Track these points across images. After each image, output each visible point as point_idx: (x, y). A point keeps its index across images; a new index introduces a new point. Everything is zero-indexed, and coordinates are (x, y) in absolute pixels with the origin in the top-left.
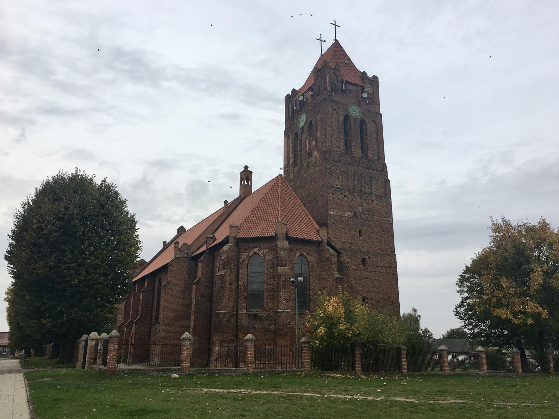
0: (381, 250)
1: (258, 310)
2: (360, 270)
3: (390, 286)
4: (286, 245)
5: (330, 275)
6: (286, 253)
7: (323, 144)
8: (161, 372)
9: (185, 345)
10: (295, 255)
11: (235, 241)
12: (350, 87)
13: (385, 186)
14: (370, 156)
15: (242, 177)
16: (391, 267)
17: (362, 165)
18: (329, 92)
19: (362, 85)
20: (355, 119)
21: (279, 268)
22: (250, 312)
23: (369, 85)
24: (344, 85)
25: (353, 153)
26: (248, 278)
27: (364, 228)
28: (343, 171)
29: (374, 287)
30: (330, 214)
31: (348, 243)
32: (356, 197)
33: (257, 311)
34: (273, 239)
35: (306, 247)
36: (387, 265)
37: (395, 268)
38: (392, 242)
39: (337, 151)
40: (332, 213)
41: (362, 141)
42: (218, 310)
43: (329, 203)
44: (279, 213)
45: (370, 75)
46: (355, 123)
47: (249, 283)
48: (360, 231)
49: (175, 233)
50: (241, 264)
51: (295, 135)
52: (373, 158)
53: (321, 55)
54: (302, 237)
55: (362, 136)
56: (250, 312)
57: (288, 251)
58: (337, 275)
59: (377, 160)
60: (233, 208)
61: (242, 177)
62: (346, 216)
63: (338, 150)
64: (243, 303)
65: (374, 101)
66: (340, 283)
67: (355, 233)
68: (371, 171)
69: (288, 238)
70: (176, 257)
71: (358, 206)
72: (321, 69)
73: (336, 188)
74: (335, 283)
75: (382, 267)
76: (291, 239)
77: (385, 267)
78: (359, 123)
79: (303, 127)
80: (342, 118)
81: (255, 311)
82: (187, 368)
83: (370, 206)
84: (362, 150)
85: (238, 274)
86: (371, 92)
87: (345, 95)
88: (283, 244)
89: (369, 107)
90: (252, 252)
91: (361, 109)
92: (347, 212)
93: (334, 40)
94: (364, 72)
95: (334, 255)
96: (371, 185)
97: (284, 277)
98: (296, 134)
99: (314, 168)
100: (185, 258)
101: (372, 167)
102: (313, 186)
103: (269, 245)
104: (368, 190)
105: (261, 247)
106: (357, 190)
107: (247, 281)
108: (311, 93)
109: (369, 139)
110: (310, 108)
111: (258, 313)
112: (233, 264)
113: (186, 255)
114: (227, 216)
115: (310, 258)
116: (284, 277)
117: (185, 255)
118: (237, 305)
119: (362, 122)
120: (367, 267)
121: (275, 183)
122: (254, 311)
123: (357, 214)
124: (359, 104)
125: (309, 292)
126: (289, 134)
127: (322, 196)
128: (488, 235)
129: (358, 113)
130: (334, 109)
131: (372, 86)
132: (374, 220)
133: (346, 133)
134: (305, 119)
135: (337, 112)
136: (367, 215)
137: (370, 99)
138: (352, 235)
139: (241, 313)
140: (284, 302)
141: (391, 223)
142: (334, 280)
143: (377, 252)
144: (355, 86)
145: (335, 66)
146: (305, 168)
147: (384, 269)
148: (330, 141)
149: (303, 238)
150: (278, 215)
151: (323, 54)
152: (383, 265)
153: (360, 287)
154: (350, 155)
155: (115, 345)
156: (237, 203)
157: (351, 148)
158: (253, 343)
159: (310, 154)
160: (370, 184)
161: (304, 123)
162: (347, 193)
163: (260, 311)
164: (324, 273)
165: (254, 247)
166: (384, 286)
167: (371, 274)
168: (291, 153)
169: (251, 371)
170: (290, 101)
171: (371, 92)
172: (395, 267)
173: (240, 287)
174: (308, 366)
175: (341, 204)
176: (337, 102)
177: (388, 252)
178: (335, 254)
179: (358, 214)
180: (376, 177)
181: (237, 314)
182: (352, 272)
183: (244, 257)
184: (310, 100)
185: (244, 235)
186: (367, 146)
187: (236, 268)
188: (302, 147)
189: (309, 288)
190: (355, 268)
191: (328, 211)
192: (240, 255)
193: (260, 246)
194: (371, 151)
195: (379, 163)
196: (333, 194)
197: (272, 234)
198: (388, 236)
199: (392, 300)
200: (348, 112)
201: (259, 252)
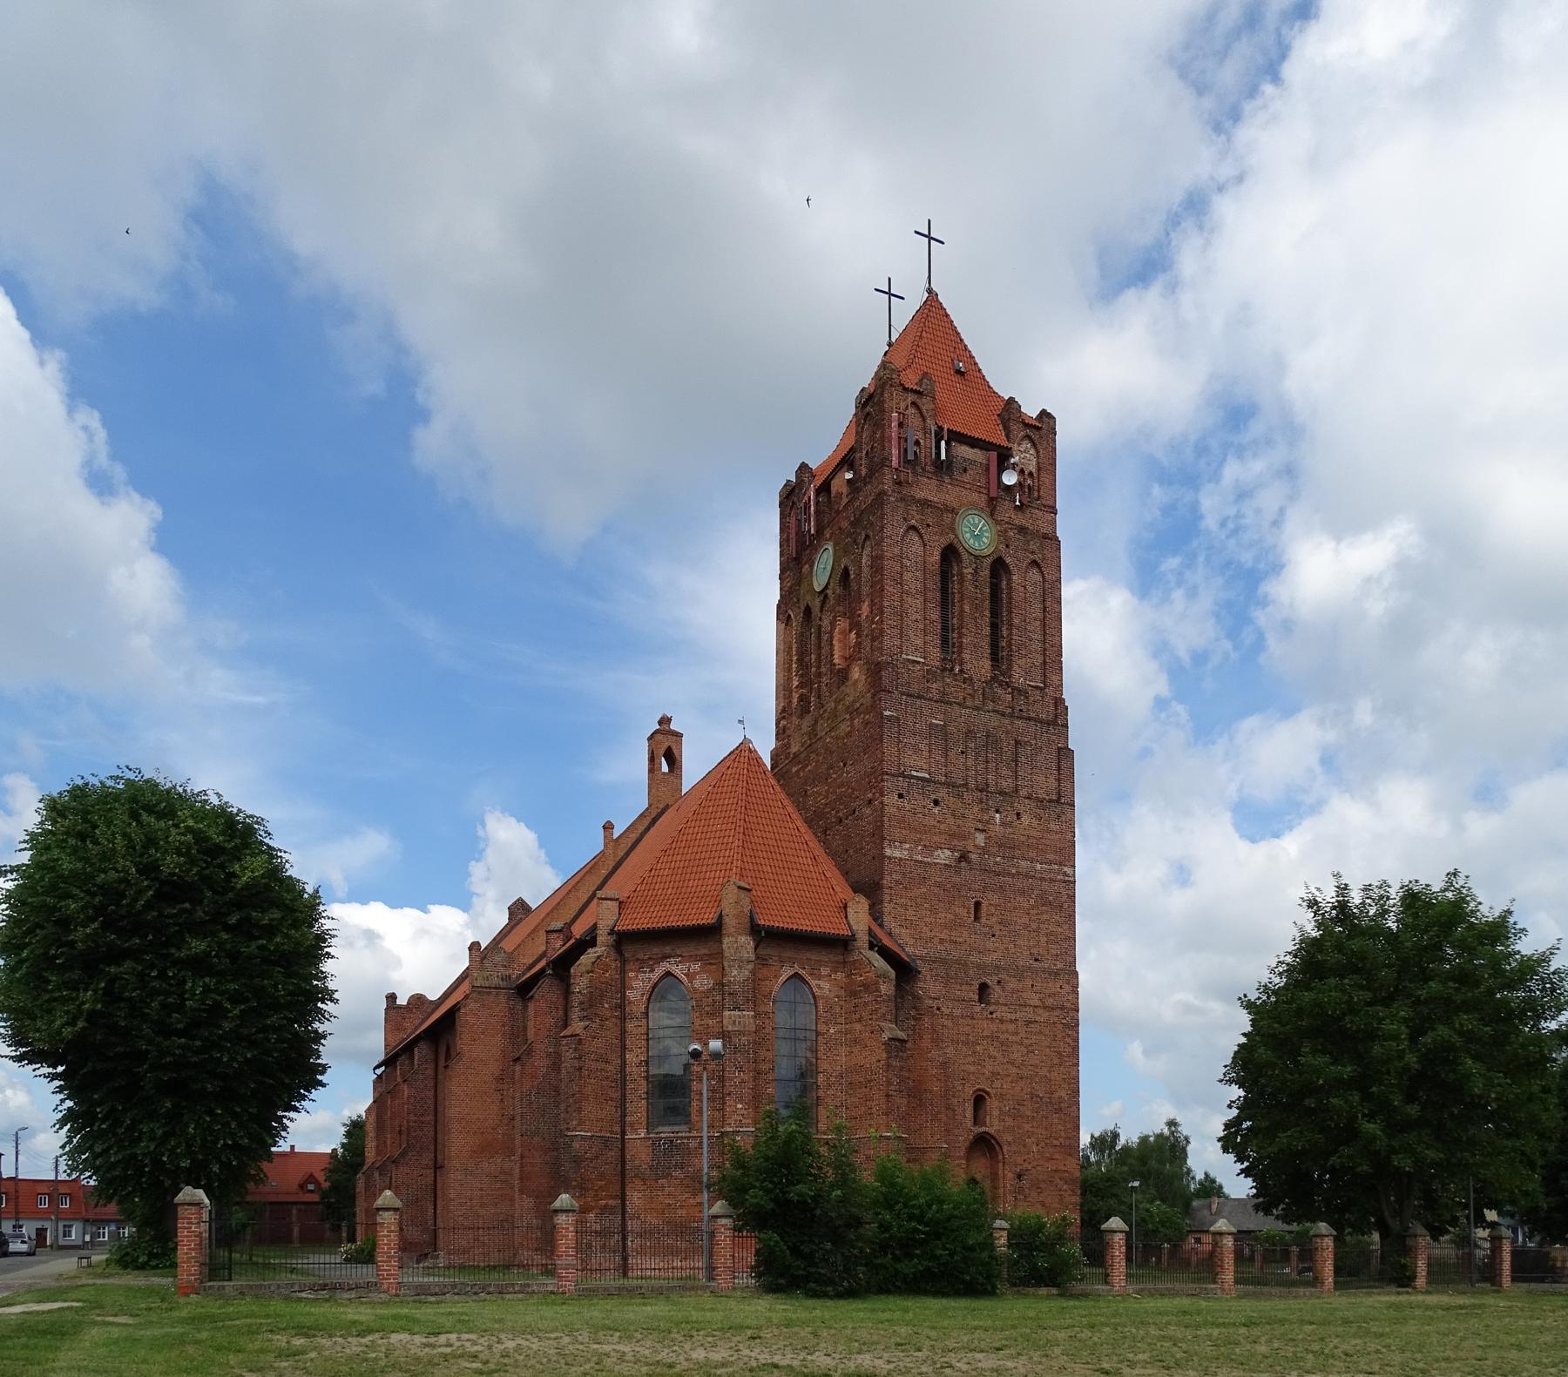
0: (1036, 960)
1: (676, 1128)
2: (973, 1018)
3: (1056, 1061)
4: (746, 948)
5: (872, 1032)
6: (747, 973)
7: (876, 643)
8: (322, 1290)
9: (384, 1223)
10: (777, 977)
11: (611, 939)
12: (964, 451)
13: (1059, 769)
14: (1019, 679)
15: (653, 751)
16: (1062, 1008)
17: (990, 706)
18: (896, 469)
19: (1005, 444)
20: (976, 557)
21: (727, 1013)
22: (657, 1133)
23: (1027, 445)
24: (943, 443)
25: (964, 666)
26: (650, 1042)
27: (990, 897)
28: (931, 724)
29: (1011, 1063)
30: (890, 858)
31: (942, 941)
32: (969, 804)
33: (673, 1133)
34: (711, 932)
35: (808, 955)
36: (1049, 1002)
37: (1072, 1009)
38: (1070, 935)
39: (918, 663)
40: (897, 854)
41: (995, 627)
42: (568, 1129)
43: (886, 824)
44: (735, 858)
45: (1031, 410)
46: (975, 570)
47: (652, 1057)
48: (978, 905)
49: (503, 920)
50: (630, 1003)
51: (804, 614)
52: (1028, 682)
53: (890, 345)
54: (795, 927)
55: (995, 613)
56: (657, 1133)
57: (751, 966)
58: (890, 1030)
59: (1037, 687)
60: (630, 845)
61: (653, 751)
62: (935, 861)
63: (922, 660)
64: (638, 1109)
65: (1039, 498)
66: (901, 1054)
67: (963, 912)
68: (1019, 723)
69: (755, 930)
70: (473, 987)
71: (973, 831)
72: (875, 391)
73: (913, 777)
74: (885, 1055)
75: (1036, 1007)
76: (763, 932)
77: (1045, 1008)
78: (987, 572)
79: (826, 587)
80: (936, 557)
81: (669, 1132)
82: (392, 1281)
83: (1010, 830)
84: (995, 657)
85: (623, 1032)
86: (1032, 467)
87: (947, 479)
88: (738, 945)
89: (1019, 519)
90: (659, 971)
91: (998, 523)
92: (939, 851)
93: (926, 292)
94: (1012, 400)
95: (884, 976)
96: (1016, 765)
97: (740, 1040)
98: (808, 611)
99: (852, 720)
100: (500, 988)
101: (1021, 710)
102: (848, 773)
103: (703, 951)
104: (1007, 784)
105: (681, 956)
106: (972, 784)
107: (648, 1051)
108: (849, 476)
109: (1016, 621)
110: (845, 524)
111: (678, 1138)
112: (606, 1006)
113: (502, 980)
114: (614, 867)
115: (819, 987)
116: (740, 1040)
117: (496, 981)
118: (624, 1116)
119: (999, 567)
120: (991, 1008)
121: (729, 768)
122: (666, 1131)
123: (970, 854)
124: (992, 504)
125: (817, 1079)
126: (790, 612)
127: (870, 802)
128: (1494, 905)
129: (987, 537)
130: (913, 528)
131: (1034, 445)
132: (1019, 873)
133: (945, 603)
134: (831, 561)
135: (921, 537)
136: (998, 859)
137: (1026, 490)
138: (953, 918)
139: (633, 1137)
140: (740, 1106)
141: (1070, 879)
142: (883, 1047)
143: (1023, 966)
144: (982, 448)
145: (920, 383)
146: (829, 718)
147: (1040, 1011)
148: (896, 631)
149: (797, 927)
150: (732, 863)
151: (893, 340)
152: (1037, 1003)
153: (969, 1064)
154: (956, 675)
155: (192, 1223)
156: (641, 828)
157: (960, 653)
158: (571, 1218)
159: (843, 675)
160: (1013, 764)
161: (828, 574)
162: (942, 793)
163: (682, 1132)
164: (858, 1026)
165: (665, 957)
166: (1038, 1062)
167: (1004, 1027)
168: (794, 674)
169: (569, 1289)
170: (794, 503)
171: (1032, 467)
172: (1073, 1006)
173: (628, 1070)
174: (729, 1275)
175: (925, 826)
176: (925, 504)
177: (1055, 965)
178: (889, 972)
179: (973, 856)
180: (1033, 742)
181: (623, 1140)
182: (949, 1023)
183: (639, 984)
184: (845, 501)
185: (637, 921)
186: (1010, 645)
187: (616, 1017)
188: (823, 652)
189: (817, 1067)
190: (957, 1012)
191: (883, 848)
192: (627, 979)
193: (678, 953)
194: (1022, 662)
195: (1043, 697)
196: (901, 796)
197: (708, 918)
198: (1057, 918)
199: (1060, 1097)
200: (957, 536)
201: (678, 970)
